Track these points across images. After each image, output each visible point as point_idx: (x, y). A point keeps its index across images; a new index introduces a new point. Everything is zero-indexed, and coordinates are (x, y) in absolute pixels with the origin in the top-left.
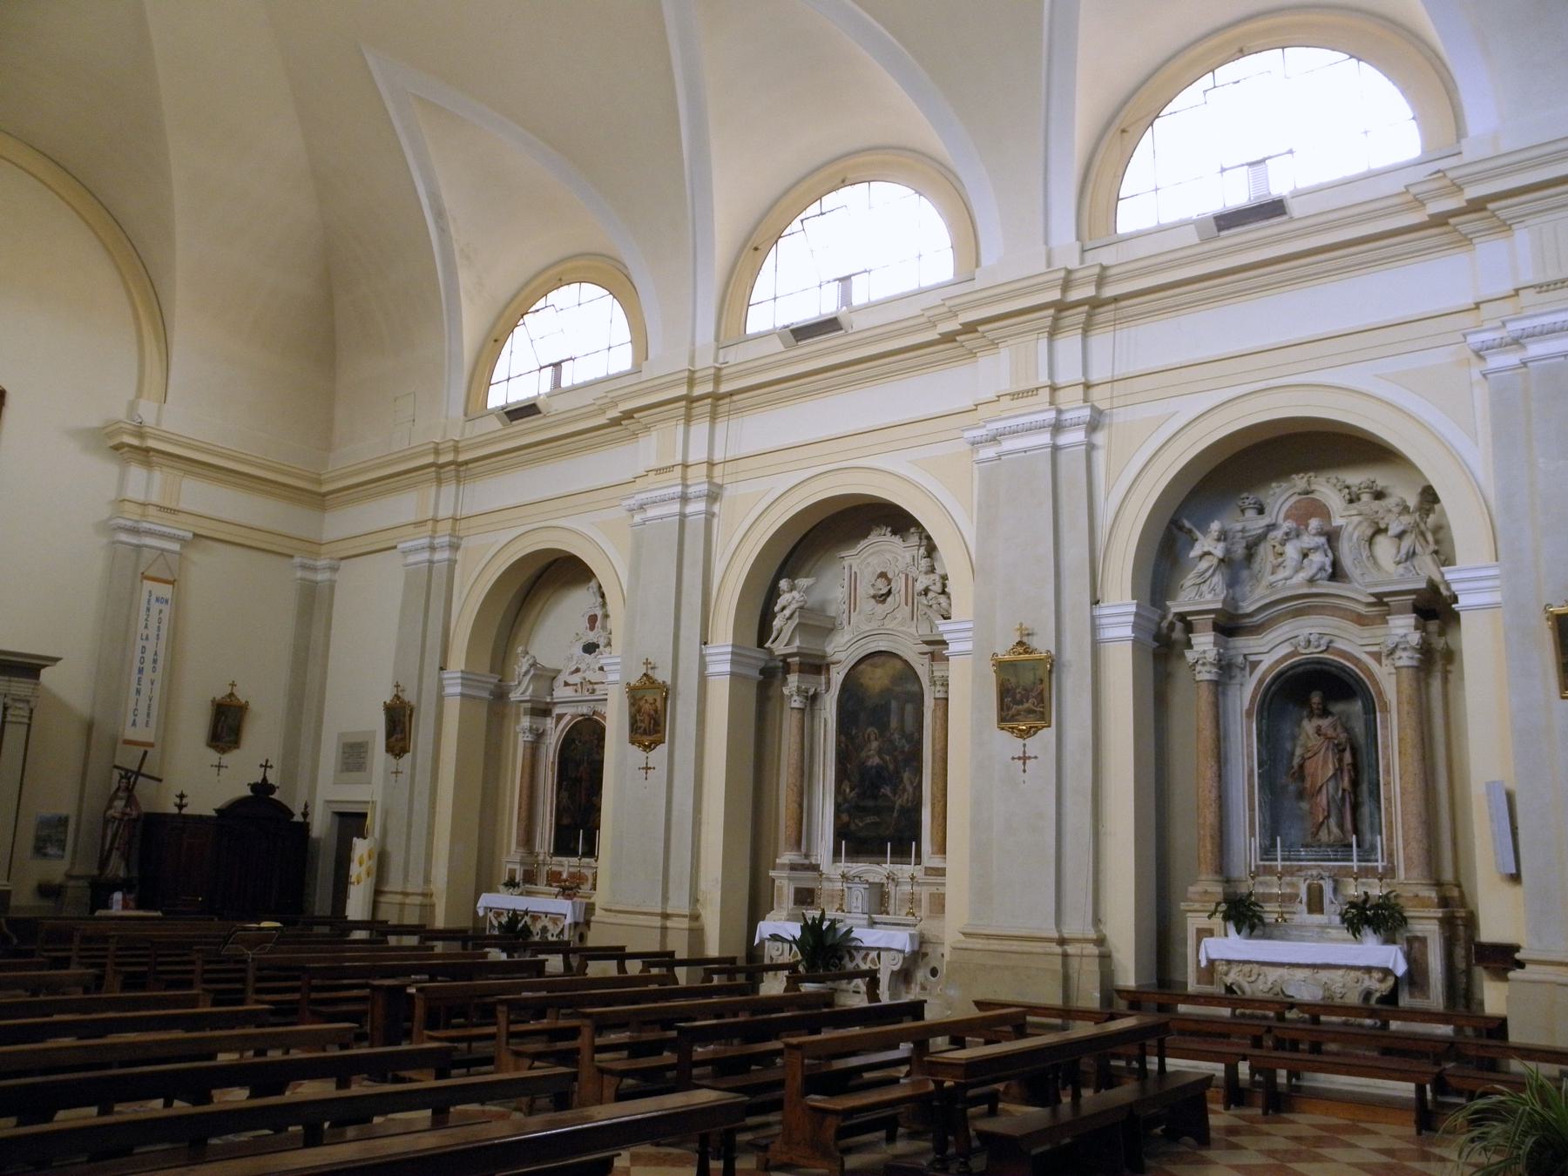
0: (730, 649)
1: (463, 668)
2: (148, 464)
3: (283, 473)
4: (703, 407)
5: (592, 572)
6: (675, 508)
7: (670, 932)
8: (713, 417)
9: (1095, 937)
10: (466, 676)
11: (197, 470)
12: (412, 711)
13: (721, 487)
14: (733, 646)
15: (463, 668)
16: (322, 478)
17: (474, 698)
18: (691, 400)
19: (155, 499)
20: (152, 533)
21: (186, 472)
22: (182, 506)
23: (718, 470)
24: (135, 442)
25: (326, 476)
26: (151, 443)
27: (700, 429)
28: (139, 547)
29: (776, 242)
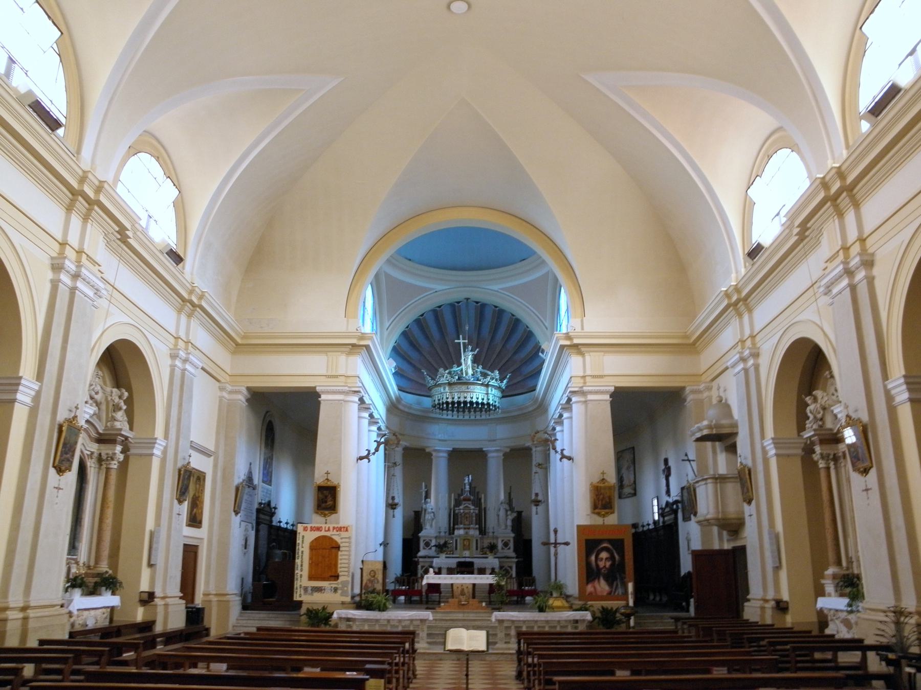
0: (902, 380)
1: (773, 436)
2: (582, 354)
3: (657, 337)
4: (844, 200)
5: (109, 346)
6: (845, 282)
7: (30, 621)
8: (856, 205)
9: (28, 611)
10: (776, 441)
11: (314, 349)
12: (750, 471)
13: (873, 254)
14: (905, 377)
15: (773, 436)
16: (688, 334)
17: (788, 456)
18: (834, 199)
19: (588, 372)
20: (340, 392)
21: (605, 352)
22: (606, 373)
23: (869, 242)
24: (568, 343)
25: (689, 332)
26: (576, 341)
27: (850, 217)
28: (585, 402)
29: (59, 55)
